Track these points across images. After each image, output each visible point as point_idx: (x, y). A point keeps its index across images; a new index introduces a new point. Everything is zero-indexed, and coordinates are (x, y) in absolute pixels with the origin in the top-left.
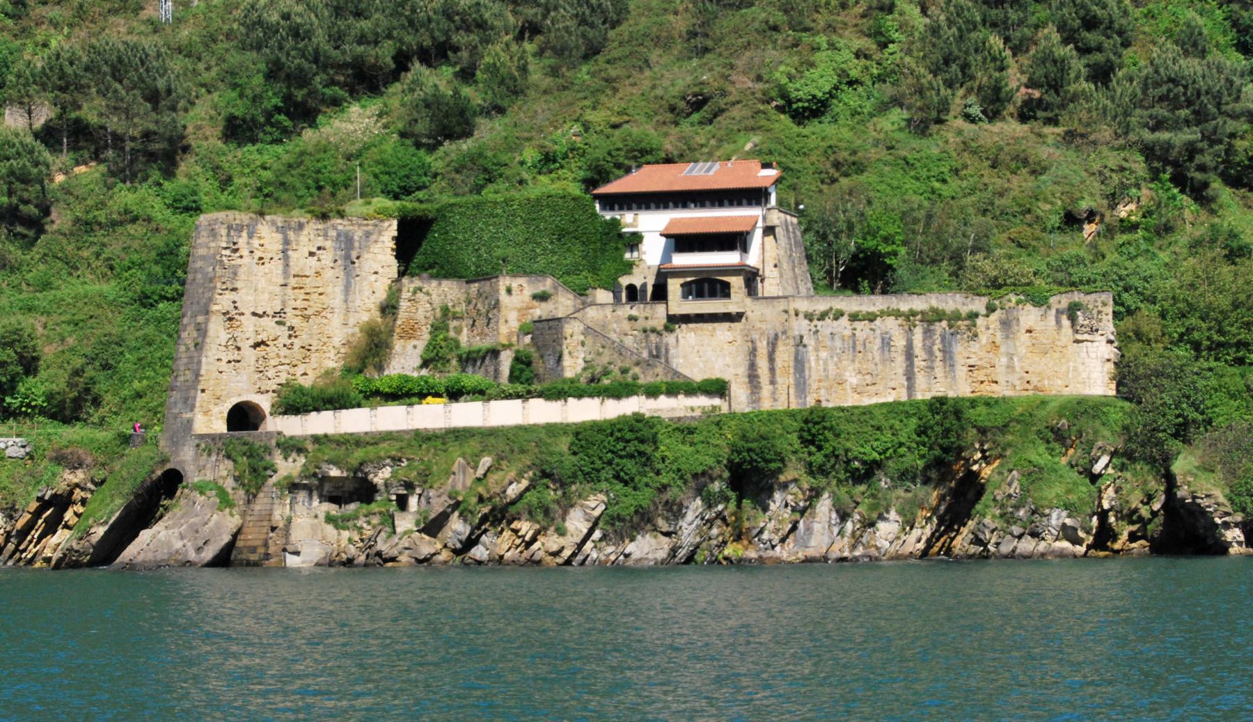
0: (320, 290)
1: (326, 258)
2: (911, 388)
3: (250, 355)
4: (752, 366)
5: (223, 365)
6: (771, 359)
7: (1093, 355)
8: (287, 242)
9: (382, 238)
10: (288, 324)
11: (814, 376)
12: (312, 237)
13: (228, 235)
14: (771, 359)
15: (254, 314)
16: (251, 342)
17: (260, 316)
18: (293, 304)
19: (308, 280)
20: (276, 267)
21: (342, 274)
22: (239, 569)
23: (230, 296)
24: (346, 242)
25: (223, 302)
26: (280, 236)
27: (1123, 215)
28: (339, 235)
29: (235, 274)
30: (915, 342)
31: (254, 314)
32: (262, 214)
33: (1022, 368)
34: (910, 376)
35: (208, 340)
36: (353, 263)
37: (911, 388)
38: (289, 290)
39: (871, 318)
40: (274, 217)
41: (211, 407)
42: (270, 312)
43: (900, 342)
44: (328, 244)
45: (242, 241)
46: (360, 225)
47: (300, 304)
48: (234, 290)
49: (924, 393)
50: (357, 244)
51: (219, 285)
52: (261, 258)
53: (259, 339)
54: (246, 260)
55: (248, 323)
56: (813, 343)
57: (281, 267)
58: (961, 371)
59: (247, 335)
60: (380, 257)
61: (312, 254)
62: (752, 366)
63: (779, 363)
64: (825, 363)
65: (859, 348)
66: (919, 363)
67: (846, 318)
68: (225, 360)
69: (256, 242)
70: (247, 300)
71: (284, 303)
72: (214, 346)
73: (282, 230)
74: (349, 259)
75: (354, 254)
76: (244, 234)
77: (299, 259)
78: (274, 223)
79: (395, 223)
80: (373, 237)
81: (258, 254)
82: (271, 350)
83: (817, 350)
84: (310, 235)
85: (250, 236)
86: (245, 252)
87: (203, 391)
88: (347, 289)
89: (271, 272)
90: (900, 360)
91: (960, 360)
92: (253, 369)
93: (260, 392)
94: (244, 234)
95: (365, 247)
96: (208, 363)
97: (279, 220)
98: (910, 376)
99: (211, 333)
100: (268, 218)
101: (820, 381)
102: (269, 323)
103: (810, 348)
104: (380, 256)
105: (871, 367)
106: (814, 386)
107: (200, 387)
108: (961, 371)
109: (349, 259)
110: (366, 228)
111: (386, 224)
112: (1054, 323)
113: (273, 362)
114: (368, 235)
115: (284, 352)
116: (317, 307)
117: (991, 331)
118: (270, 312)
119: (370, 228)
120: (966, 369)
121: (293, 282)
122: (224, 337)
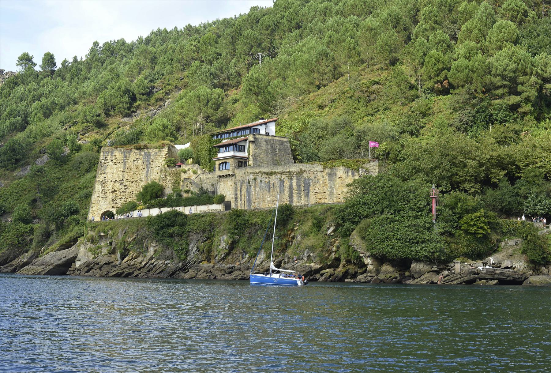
1: (140, 162)
3: (110, 195)
4: (236, 195)
5: (100, 199)
6: (241, 192)
8: (125, 157)
11: (254, 197)
13: (104, 155)
14: (241, 192)
16: (111, 191)
19: (132, 170)
20: (120, 166)
22: (73, 277)
25: (101, 178)
27: (392, 300)
32: (117, 148)
33: (337, 192)
34: (291, 196)
55: (110, 186)
58: (312, 195)
61: (134, 160)
62: (236, 195)
63: (243, 193)
66: (295, 191)
68: (101, 197)
70: (109, 176)
71: (123, 177)
76: (110, 154)
77: (130, 162)
78: (121, 151)
80: (159, 154)
81: (114, 161)
82: (118, 193)
83: (255, 187)
84: (134, 154)
88: (147, 172)
93: (113, 207)
94: (110, 154)
101: (256, 199)
103: (252, 187)
113: (118, 198)
115: (122, 194)
116: (136, 179)
121: (127, 170)
122: (101, 189)
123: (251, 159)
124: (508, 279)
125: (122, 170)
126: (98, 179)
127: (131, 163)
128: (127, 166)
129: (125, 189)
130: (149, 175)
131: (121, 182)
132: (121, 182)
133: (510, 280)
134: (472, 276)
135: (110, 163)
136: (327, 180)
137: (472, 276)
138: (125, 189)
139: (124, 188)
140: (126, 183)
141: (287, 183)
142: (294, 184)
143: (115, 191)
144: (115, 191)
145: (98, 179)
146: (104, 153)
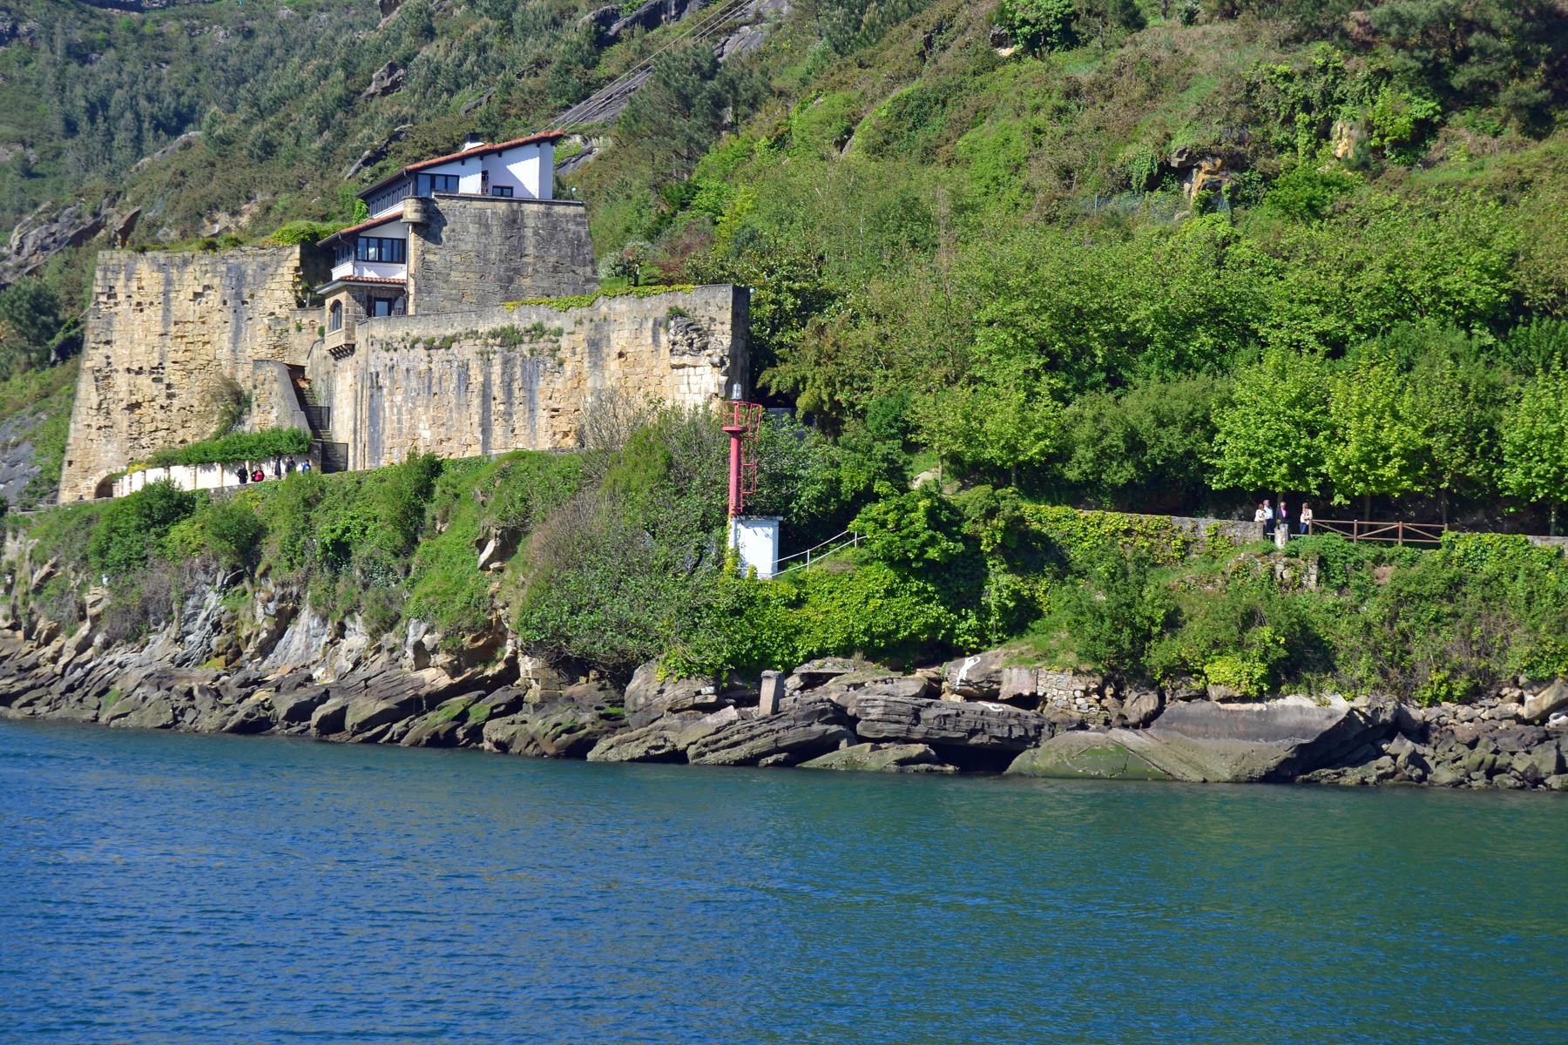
0: (206, 338)
1: (213, 298)
2: (486, 444)
3: (121, 418)
7: (695, 388)
9: (280, 271)
10: (166, 381)
12: (198, 274)
13: (105, 278)
15: (129, 370)
16: (124, 404)
17: (137, 373)
18: (172, 356)
19: (190, 327)
20: (154, 314)
21: (231, 317)
23: (104, 350)
24: (238, 278)
26: (162, 276)
28: (229, 269)
29: (110, 323)
30: (494, 377)
31: (129, 370)
32: (143, 250)
34: (486, 429)
35: (77, 403)
36: (244, 303)
37: (486, 444)
38: (168, 341)
39: (447, 343)
40: (155, 253)
41: (79, 481)
42: (146, 368)
43: (476, 378)
44: (216, 281)
45: (119, 286)
46: (255, 255)
47: (180, 356)
48: (108, 343)
49: (500, 444)
50: (250, 279)
51: (91, 338)
52: (139, 304)
53: (134, 399)
54: (124, 307)
55: (121, 381)
56: (388, 383)
57: (160, 313)
58: (542, 417)
59: (121, 396)
60: (278, 294)
61: (197, 295)
64: (399, 413)
65: (435, 389)
66: (498, 407)
67: (420, 346)
69: (134, 285)
71: (162, 356)
72: (83, 410)
73: (161, 268)
74: (239, 300)
75: (246, 292)
76: (122, 276)
77: (182, 304)
78: (154, 259)
79: (297, 249)
80: (271, 270)
81: (136, 298)
83: (391, 393)
85: (128, 279)
86: (121, 297)
87: (70, 463)
88: (237, 332)
89: (149, 320)
90: (476, 402)
91: (542, 402)
92: (125, 435)
94: (122, 276)
95: (260, 282)
96: (77, 430)
97: (162, 257)
98: (486, 429)
99: (82, 394)
100: (149, 254)
102: (145, 380)
103: (385, 391)
104: (279, 289)
105: (445, 415)
106: (388, 443)
107: (67, 458)
108: (542, 417)
109: (239, 300)
110: (260, 259)
111: (288, 251)
112: (650, 340)
113: (148, 428)
114: (264, 267)
115: (160, 415)
117: (578, 357)
118: (146, 368)
119: (267, 258)
120: (546, 414)
121: (173, 329)
123: (412, 282)
124: (973, 741)
125: (160, 329)
126: (89, 364)
127: (187, 303)
128: (176, 313)
129: (170, 396)
130: (241, 345)
131: (156, 372)
132: (156, 372)
133: (979, 748)
134: (817, 728)
135: (124, 307)
136: (586, 364)
137: (817, 728)
138: (170, 396)
139: (164, 392)
140: (172, 375)
141: (476, 378)
142: (496, 378)
143: (138, 405)
144: (138, 405)
145: (89, 364)
146: (106, 270)
